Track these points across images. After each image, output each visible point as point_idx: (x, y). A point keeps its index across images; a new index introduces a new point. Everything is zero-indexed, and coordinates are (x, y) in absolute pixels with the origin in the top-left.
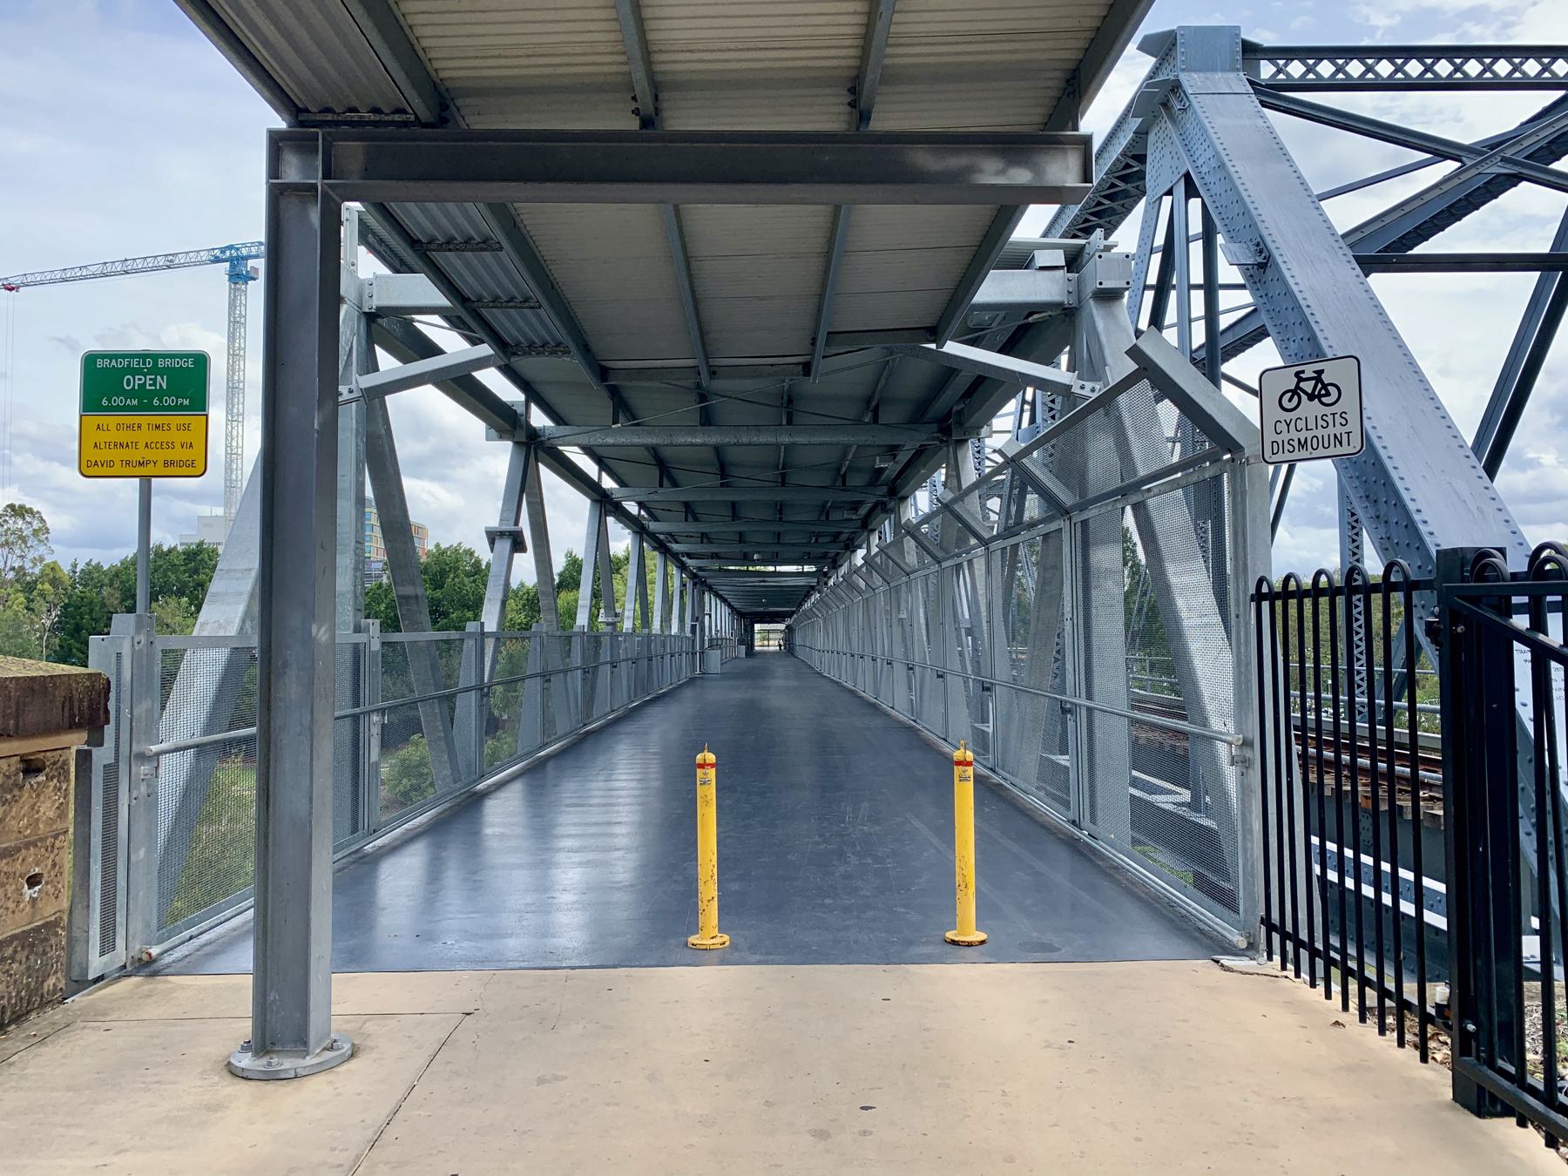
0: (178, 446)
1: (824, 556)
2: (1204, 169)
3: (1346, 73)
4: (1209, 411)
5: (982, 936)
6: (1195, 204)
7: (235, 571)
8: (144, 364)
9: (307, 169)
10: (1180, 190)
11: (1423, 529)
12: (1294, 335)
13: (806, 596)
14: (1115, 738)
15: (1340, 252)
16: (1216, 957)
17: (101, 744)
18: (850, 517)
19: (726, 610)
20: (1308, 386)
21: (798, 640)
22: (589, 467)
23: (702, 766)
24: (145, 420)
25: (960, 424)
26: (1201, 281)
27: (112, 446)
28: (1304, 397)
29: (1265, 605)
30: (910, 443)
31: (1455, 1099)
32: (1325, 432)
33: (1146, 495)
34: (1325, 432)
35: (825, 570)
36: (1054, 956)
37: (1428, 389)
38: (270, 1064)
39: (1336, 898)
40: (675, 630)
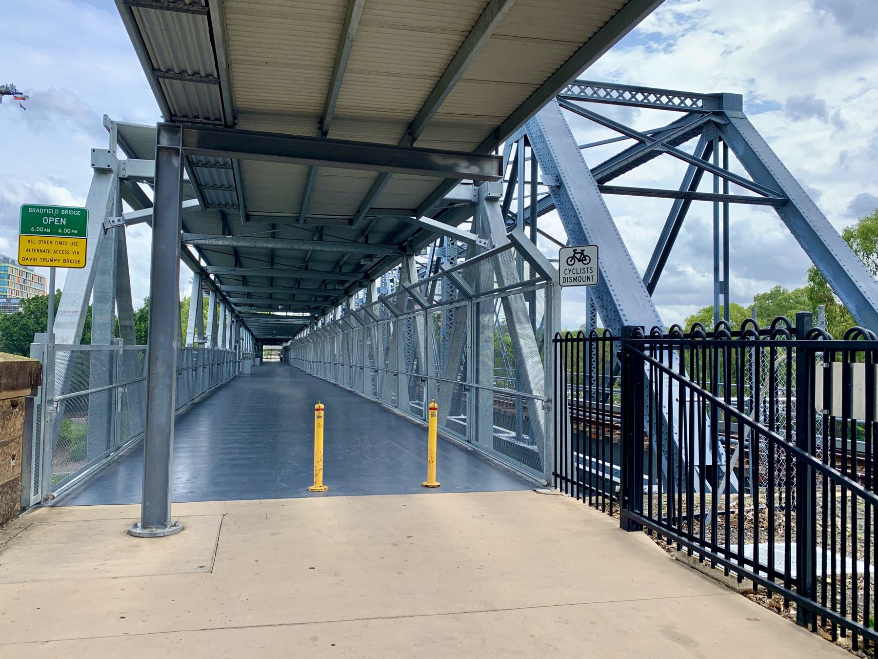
0: (71, 253)
1: (317, 308)
2: (534, 136)
3: (598, 94)
4: (539, 263)
5: (438, 484)
6: (528, 150)
7: (69, 312)
8: (54, 212)
9: (171, 140)
10: (522, 142)
11: (621, 313)
12: (571, 220)
13: (300, 330)
14: (487, 402)
15: (592, 184)
16: (534, 489)
17: (36, 395)
18: (339, 288)
19: (250, 337)
20: (578, 256)
21: (292, 355)
22: (196, 254)
23: (318, 410)
24: (54, 239)
25: (411, 247)
26: (529, 180)
27: (36, 251)
28: (576, 260)
29: (558, 344)
30: (380, 253)
31: (620, 527)
32: (584, 275)
33: (509, 294)
34: (584, 275)
35: (316, 316)
36: (469, 490)
37: (626, 251)
38: (152, 531)
39: (582, 474)
40: (227, 347)
